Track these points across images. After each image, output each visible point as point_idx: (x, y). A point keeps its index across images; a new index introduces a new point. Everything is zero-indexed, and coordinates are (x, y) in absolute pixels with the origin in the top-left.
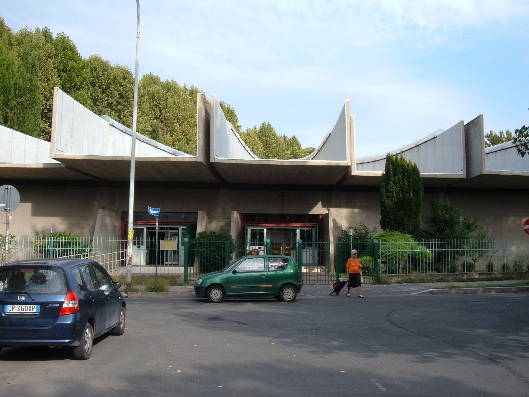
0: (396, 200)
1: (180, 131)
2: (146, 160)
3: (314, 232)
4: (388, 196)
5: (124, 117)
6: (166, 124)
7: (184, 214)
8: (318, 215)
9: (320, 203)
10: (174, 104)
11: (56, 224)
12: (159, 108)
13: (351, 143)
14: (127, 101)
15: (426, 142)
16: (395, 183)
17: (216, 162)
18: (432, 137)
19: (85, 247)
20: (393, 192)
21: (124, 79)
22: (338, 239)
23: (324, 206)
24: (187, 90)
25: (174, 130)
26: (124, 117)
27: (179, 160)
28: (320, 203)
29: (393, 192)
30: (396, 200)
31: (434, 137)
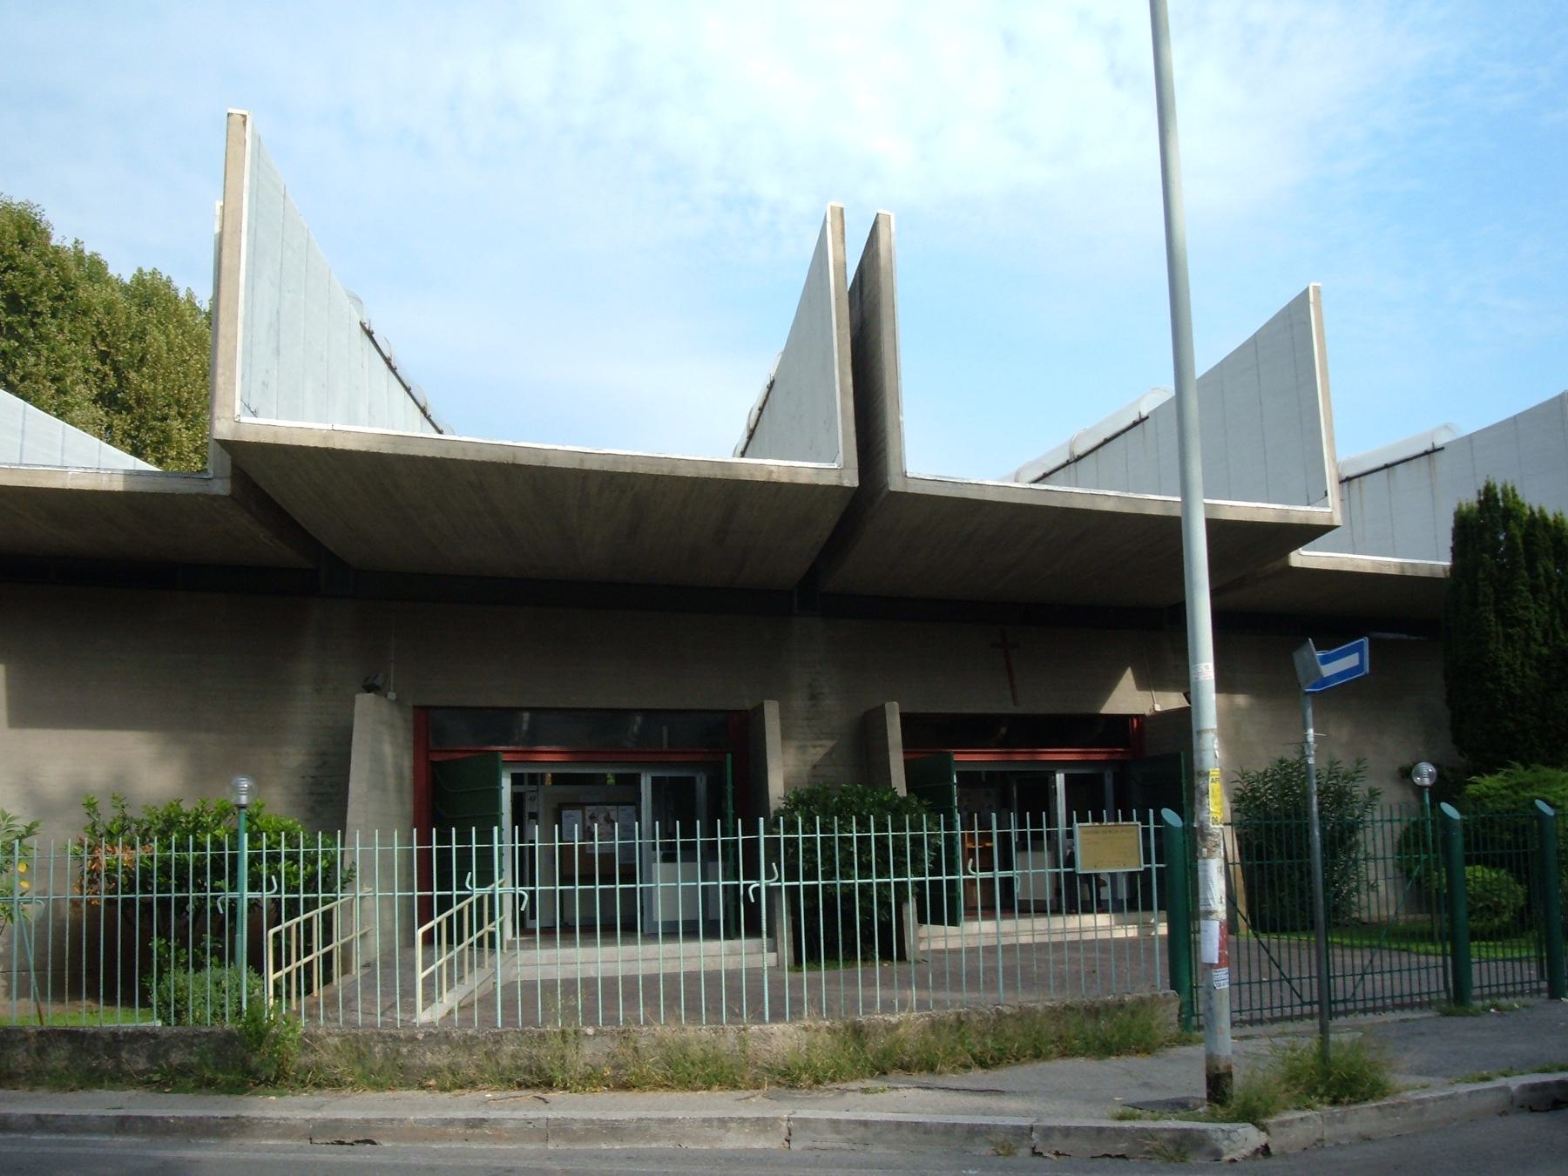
0: (1545, 651)
1: (187, 447)
2: (641, 470)
3: (1109, 782)
4: (1509, 637)
5: (23, 379)
6: (142, 417)
7: (526, 716)
8: (1123, 720)
9: (1129, 673)
10: (169, 350)
11: (134, 765)
12: (114, 362)
13: (1331, 439)
14: (33, 325)
15: (1387, 466)
16: (1535, 590)
17: (910, 490)
18: (1421, 450)
19: (936, 871)
20: (1529, 622)
21: (24, 243)
22: (1245, 804)
23: (1145, 683)
24: (200, 312)
25: (167, 439)
26: (23, 379)
27: (775, 478)
28: (1129, 673)
29: (1529, 622)
30: (1545, 651)
31: (1429, 447)
